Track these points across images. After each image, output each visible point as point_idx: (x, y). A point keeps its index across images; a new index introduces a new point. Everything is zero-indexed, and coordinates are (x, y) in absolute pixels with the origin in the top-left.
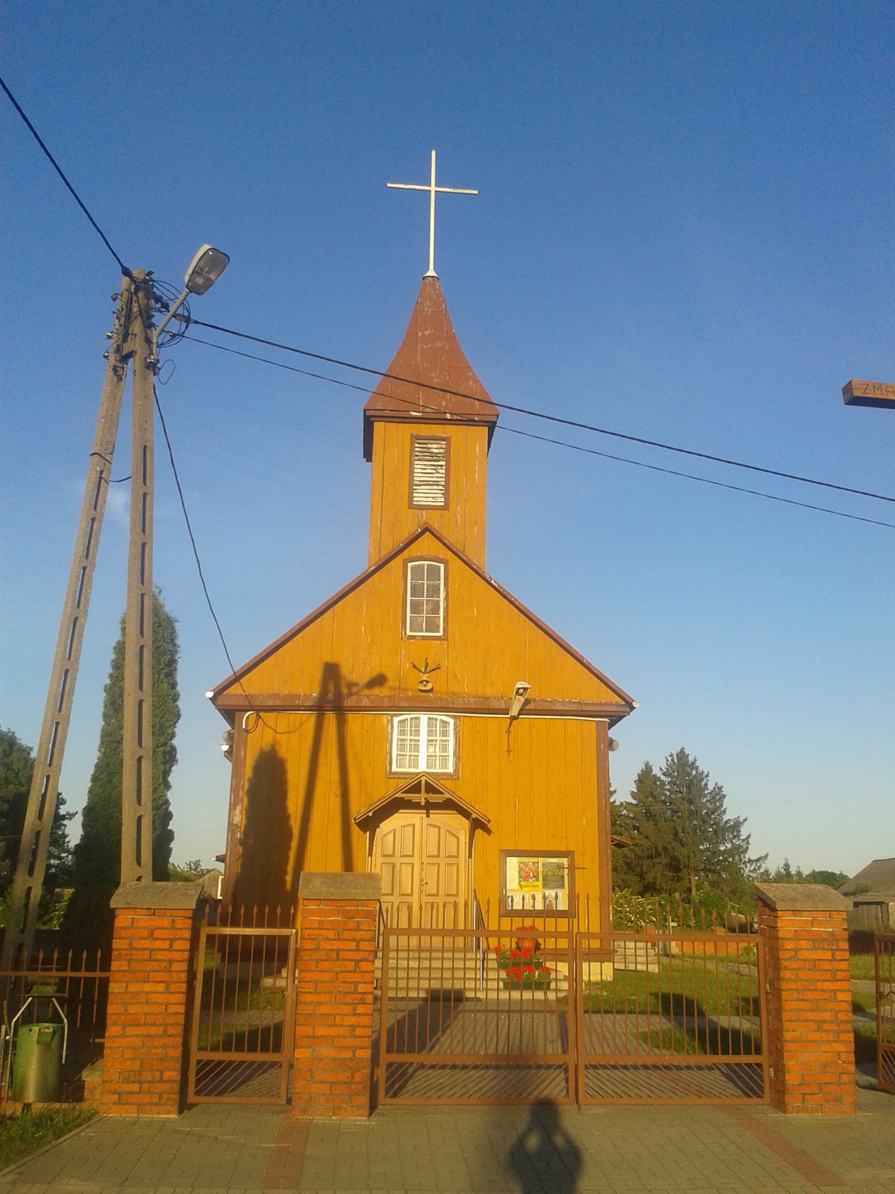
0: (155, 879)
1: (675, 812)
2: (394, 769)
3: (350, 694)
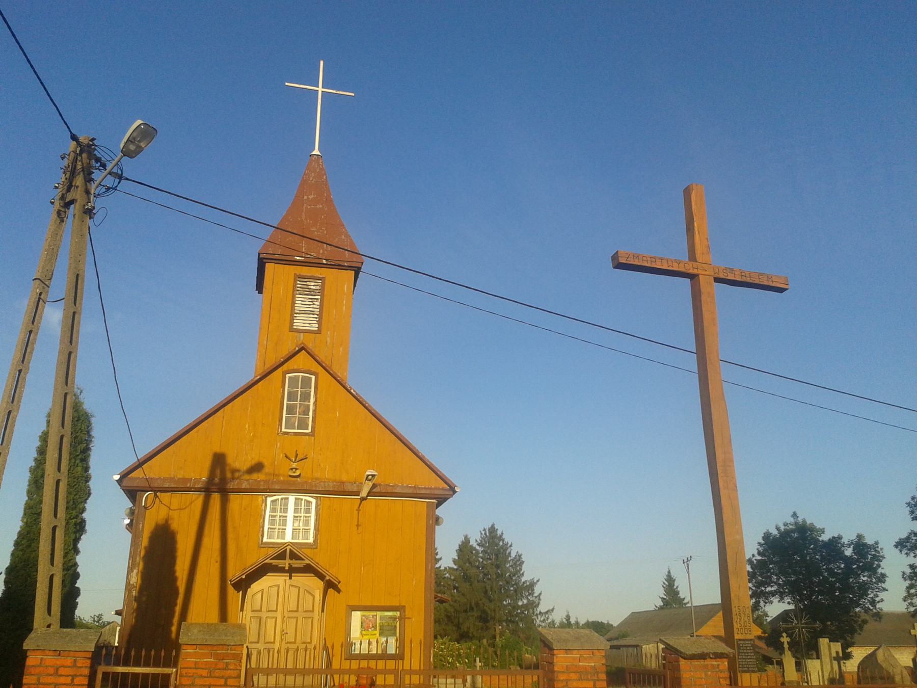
0: (61, 627)
1: (486, 575)
2: (265, 540)
3: (233, 479)
